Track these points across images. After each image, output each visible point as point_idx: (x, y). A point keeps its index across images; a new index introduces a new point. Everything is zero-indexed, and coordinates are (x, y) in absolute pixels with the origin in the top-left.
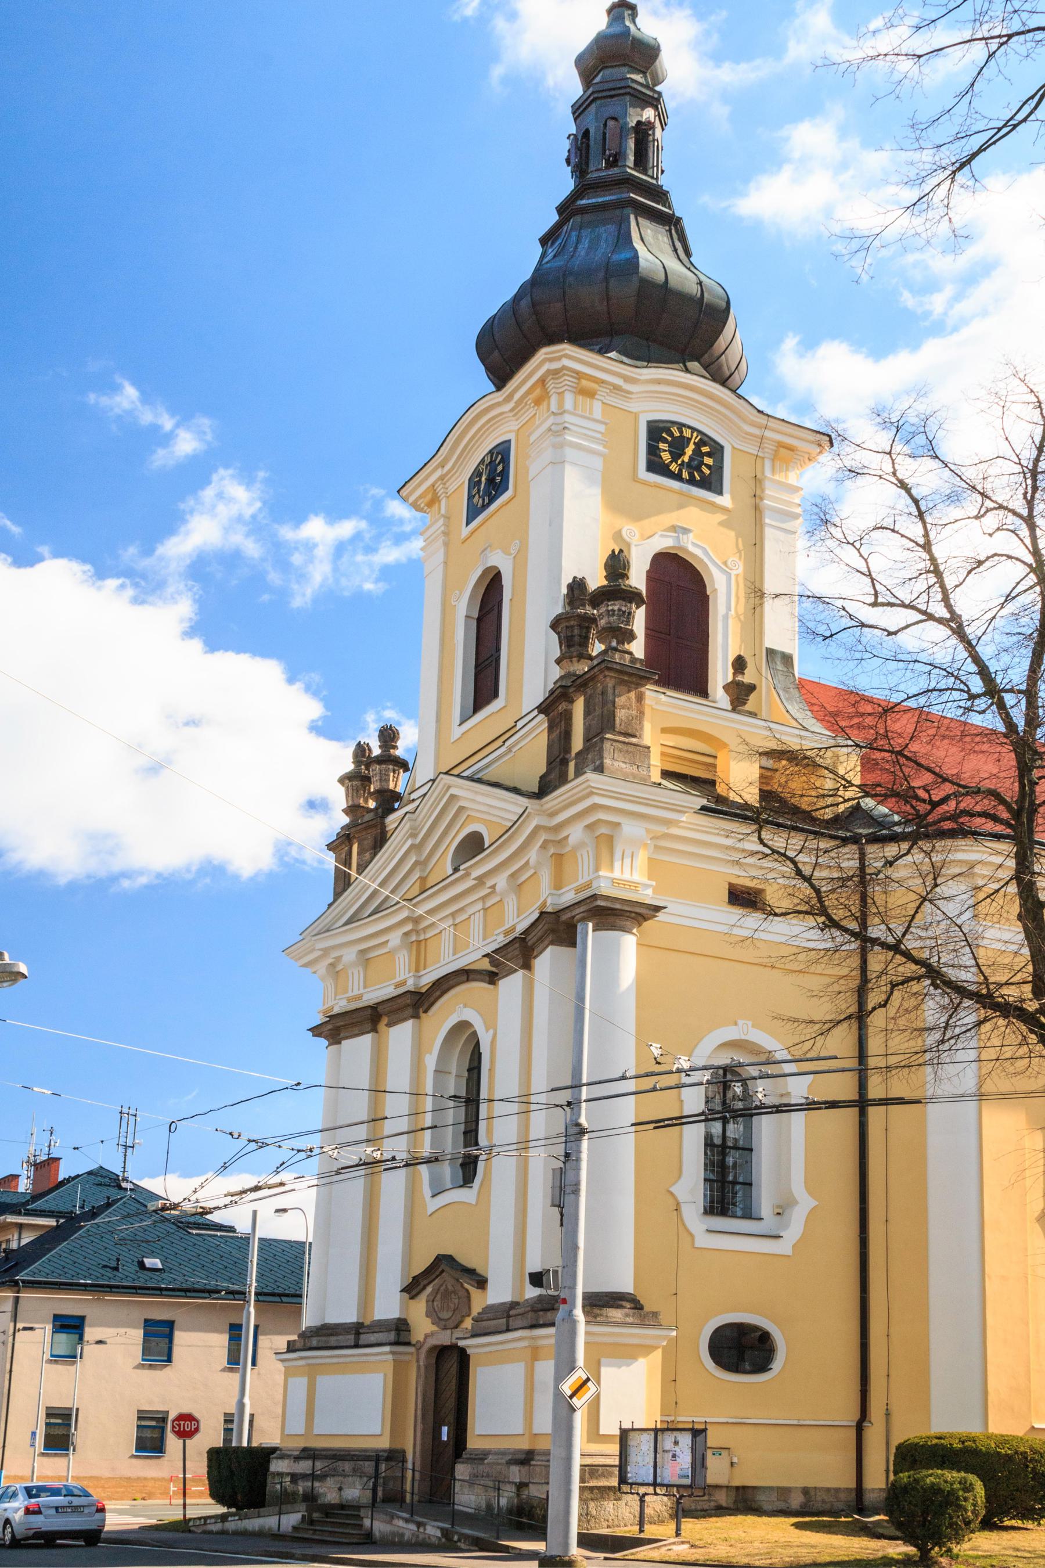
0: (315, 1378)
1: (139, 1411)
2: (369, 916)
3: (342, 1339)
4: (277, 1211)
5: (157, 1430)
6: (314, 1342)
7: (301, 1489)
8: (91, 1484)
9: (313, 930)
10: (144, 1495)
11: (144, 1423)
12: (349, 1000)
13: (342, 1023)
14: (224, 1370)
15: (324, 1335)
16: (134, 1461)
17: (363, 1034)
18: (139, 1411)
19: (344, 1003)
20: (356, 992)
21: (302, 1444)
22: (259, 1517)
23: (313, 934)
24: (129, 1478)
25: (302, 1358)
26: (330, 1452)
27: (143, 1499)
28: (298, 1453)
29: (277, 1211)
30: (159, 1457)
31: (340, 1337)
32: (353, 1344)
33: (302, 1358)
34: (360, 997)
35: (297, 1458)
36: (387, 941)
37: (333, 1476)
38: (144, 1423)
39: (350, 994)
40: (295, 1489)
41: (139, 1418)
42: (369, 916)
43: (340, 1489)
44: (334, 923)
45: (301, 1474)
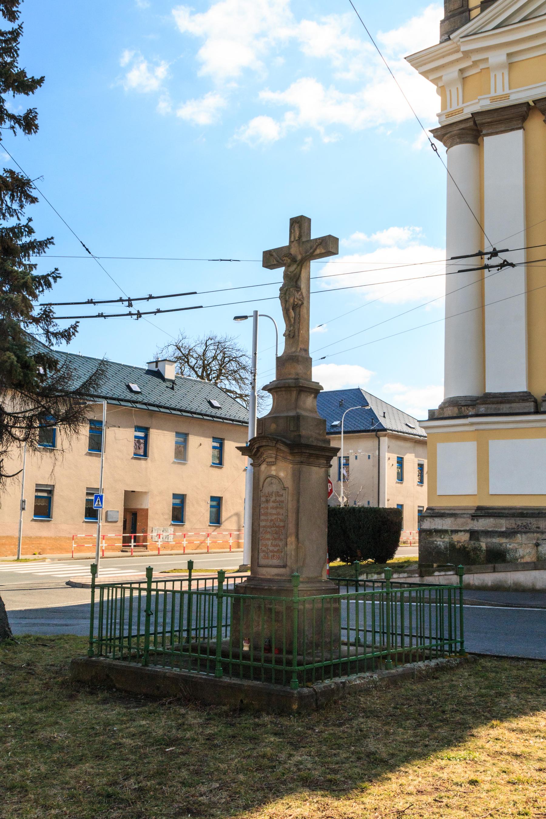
0: (488, 443)
1: (37, 485)
2: (520, 21)
3: (517, 407)
4: (236, 318)
5: (43, 500)
6: (482, 409)
7: (483, 546)
8: (7, 542)
9: (462, 33)
10: (40, 550)
11: (40, 494)
12: (493, 99)
13: (489, 120)
14: (86, 454)
15: (493, 403)
16: (34, 523)
17: (513, 130)
18: (37, 485)
19: (488, 102)
20: (500, 92)
21: (474, 503)
22: (494, 572)
23: (462, 36)
24: (31, 538)
25: (472, 424)
26: (514, 511)
27: (40, 554)
28: (473, 511)
29: (236, 318)
30: (49, 521)
31: (514, 405)
32: (532, 410)
33: (472, 424)
34: (507, 97)
35: (474, 517)
36: (487, 59)
37: (525, 533)
38: (40, 494)
39: (493, 94)
40: (477, 545)
41: (37, 490)
42: (520, 21)
43: (537, 545)
44: (482, 28)
45: (483, 532)
